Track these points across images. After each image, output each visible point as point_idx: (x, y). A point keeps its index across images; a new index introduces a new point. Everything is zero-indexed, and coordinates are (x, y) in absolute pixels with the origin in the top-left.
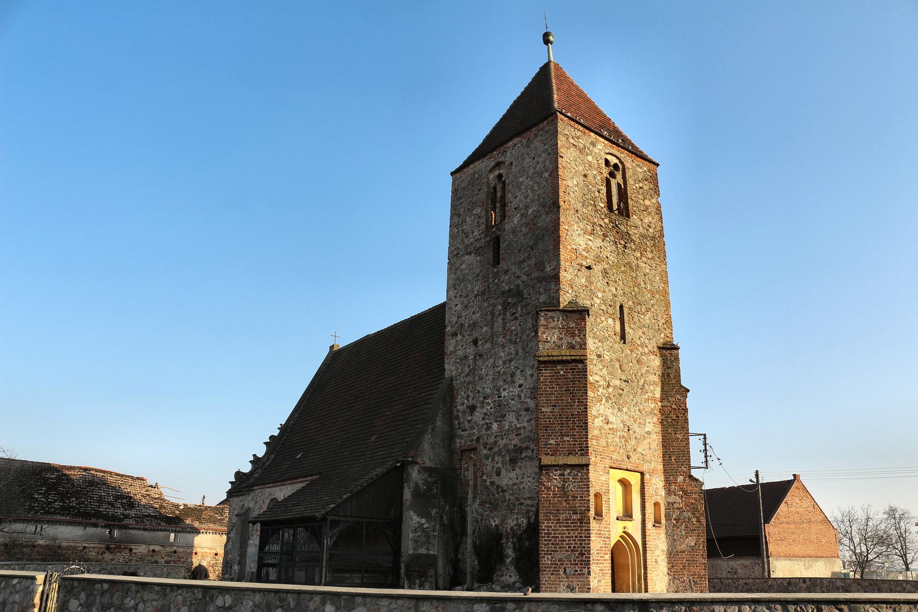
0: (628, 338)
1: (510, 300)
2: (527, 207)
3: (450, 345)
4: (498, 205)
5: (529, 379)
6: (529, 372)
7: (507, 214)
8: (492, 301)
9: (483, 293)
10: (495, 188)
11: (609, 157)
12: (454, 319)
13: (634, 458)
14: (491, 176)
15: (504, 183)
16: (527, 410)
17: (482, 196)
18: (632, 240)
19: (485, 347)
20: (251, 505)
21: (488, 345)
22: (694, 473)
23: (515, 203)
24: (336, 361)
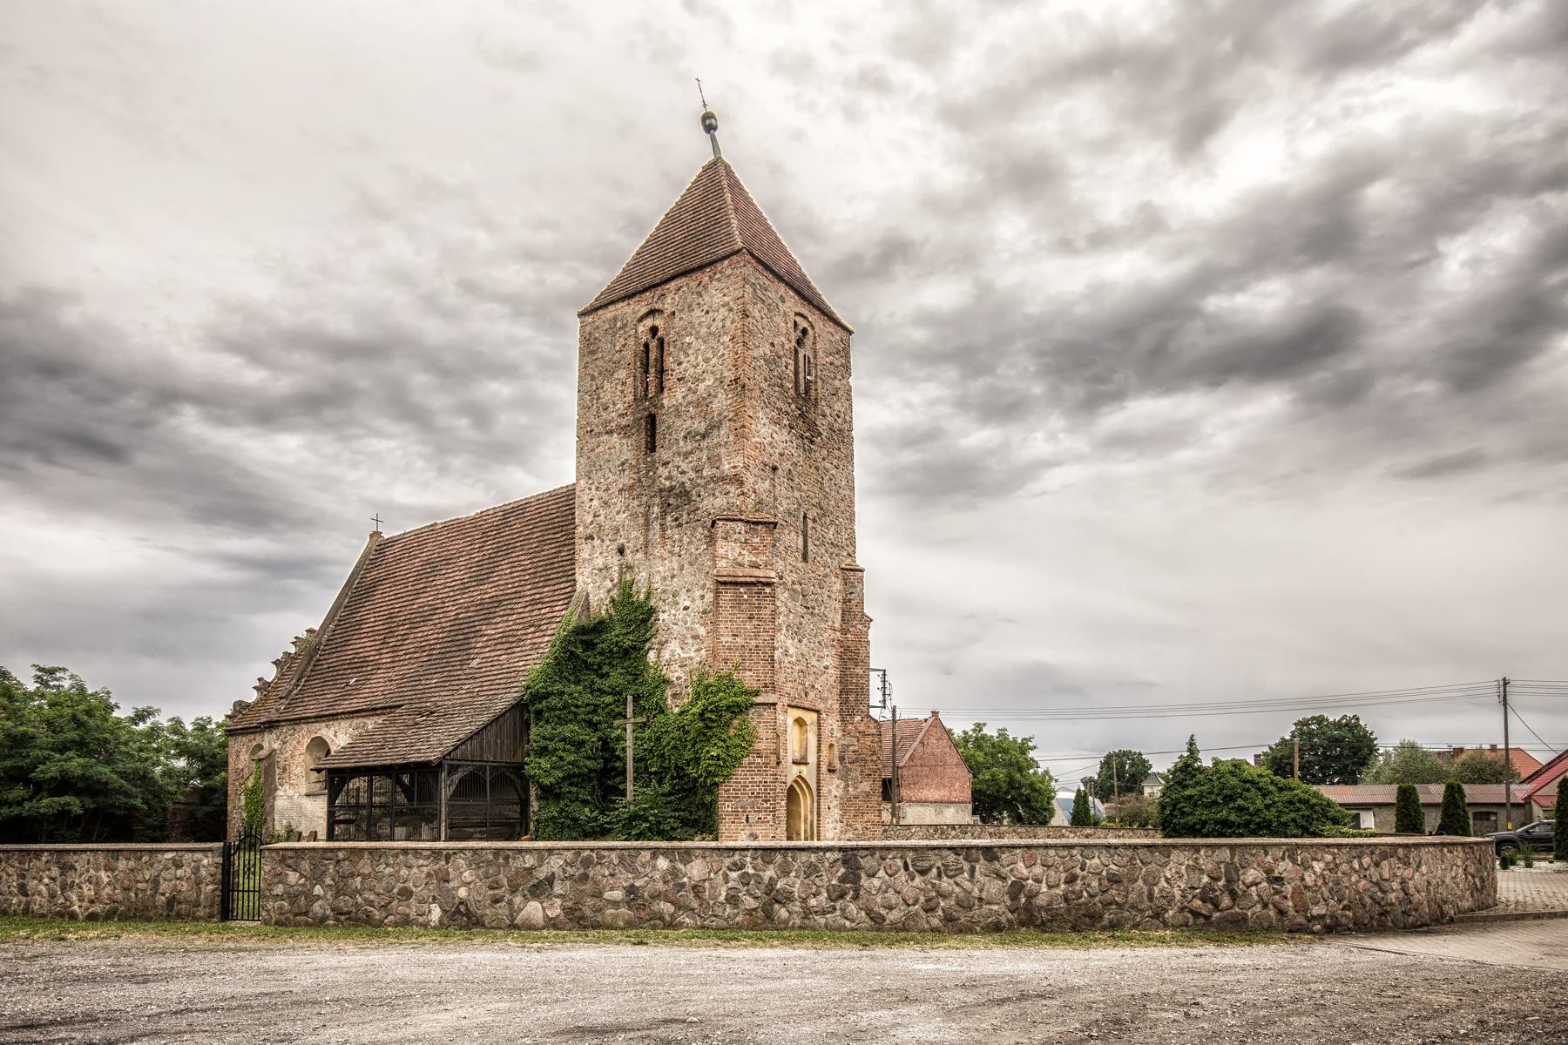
0: (811, 555)
1: (671, 501)
2: (698, 380)
3: (584, 551)
4: (652, 370)
5: (698, 602)
6: (698, 593)
7: (666, 384)
8: (644, 499)
9: (631, 487)
10: (646, 346)
11: (799, 319)
13: (812, 695)
15: (661, 341)
16: (695, 637)
17: (628, 354)
20: (276, 746)
21: (640, 555)
23: (678, 370)
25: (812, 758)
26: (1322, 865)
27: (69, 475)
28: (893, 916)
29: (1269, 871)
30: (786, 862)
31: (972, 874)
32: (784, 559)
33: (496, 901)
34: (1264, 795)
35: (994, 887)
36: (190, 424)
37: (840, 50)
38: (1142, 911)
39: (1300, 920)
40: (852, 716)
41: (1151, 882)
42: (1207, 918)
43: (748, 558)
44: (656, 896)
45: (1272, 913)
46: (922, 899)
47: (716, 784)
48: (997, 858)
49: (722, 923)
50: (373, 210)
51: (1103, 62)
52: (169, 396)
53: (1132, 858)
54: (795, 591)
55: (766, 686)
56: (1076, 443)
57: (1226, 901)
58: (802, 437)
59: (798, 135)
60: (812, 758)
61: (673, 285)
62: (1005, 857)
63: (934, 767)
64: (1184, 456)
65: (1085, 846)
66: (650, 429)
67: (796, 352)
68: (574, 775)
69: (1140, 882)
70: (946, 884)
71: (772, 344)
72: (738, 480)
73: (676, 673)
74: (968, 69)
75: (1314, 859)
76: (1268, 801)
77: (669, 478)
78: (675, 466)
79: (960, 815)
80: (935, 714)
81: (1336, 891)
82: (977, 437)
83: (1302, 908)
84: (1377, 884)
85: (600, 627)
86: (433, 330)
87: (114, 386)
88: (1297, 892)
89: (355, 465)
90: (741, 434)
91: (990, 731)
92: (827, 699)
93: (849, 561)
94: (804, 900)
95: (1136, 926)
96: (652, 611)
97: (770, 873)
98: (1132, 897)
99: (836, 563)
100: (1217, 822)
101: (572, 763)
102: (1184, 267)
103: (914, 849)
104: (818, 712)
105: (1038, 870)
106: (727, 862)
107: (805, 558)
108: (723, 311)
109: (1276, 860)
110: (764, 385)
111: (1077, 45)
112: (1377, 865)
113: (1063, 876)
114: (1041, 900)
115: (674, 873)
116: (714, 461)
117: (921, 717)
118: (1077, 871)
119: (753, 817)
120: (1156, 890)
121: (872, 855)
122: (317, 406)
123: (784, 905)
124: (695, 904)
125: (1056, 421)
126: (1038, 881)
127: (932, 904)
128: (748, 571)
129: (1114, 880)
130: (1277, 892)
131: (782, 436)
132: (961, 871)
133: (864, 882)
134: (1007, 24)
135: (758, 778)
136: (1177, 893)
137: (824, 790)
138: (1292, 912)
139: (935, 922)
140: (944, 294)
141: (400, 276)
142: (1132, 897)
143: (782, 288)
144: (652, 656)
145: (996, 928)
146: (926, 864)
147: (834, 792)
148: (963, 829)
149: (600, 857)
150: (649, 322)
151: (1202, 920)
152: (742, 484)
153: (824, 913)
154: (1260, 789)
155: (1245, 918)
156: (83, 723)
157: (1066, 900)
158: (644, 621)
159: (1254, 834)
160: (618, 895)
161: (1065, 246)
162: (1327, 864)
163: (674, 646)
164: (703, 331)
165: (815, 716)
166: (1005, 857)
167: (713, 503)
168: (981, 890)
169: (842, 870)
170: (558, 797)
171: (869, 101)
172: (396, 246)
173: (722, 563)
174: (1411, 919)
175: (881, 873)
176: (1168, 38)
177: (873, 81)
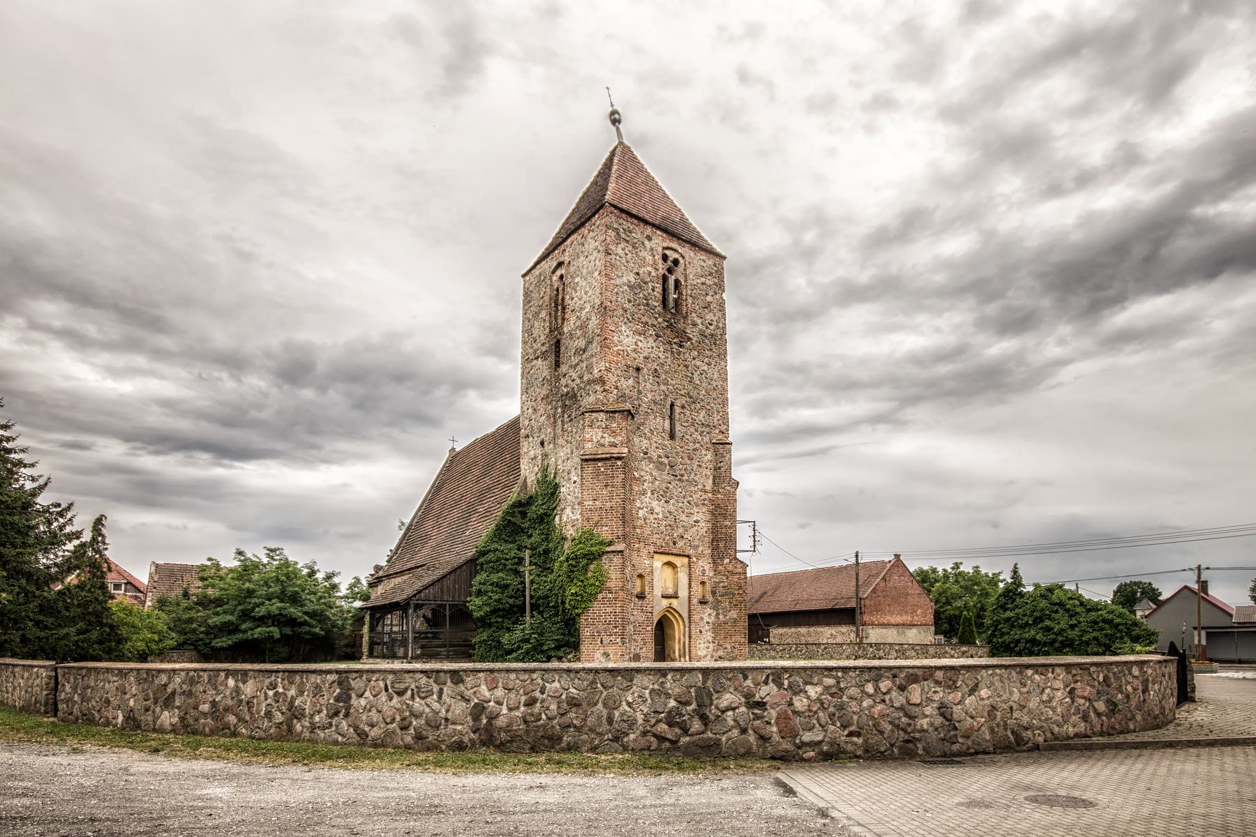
2: (582, 309)
11: (668, 252)
12: (527, 423)
13: (680, 543)
14: (555, 278)
18: (689, 339)
19: (549, 447)
22: (739, 556)
24: (455, 459)
25: (683, 593)
26: (819, 689)
28: (374, 733)
29: (748, 696)
30: (302, 683)
31: (440, 697)
32: (649, 439)
33: (147, 710)
34: (1071, 616)
35: (459, 708)
37: (857, 85)
38: (600, 734)
39: (786, 745)
40: (722, 559)
41: (611, 705)
42: (674, 742)
43: (608, 439)
44: (227, 710)
45: (752, 738)
46: (398, 718)
47: (578, 615)
48: (462, 681)
49: (262, 734)
51: (1072, 46)
53: (593, 682)
54: (661, 463)
55: (618, 537)
56: (1086, 343)
57: (696, 725)
58: (670, 343)
59: (832, 152)
60: (683, 593)
61: (569, 241)
62: (469, 680)
63: (898, 599)
64: (1184, 344)
65: (546, 670)
66: (556, 348)
67: (665, 279)
68: (499, 610)
69: (600, 705)
70: (418, 704)
71: (638, 274)
72: (602, 381)
73: (570, 532)
74: (957, 77)
75: (806, 683)
76: (1074, 622)
77: (566, 386)
78: (571, 377)
79: (927, 636)
80: (897, 556)
81: (840, 716)
82: (999, 348)
83: (789, 732)
84: (901, 708)
85: (531, 500)
88: (783, 718)
90: (605, 344)
91: (967, 568)
92: (697, 547)
93: (720, 437)
94: (312, 716)
95: (594, 749)
96: (557, 486)
97: (292, 692)
98: (591, 721)
99: (707, 439)
100: (1027, 641)
101: (498, 601)
102: (1168, 188)
103: (393, 672)
104: (688, 556)
105: (500, 692)
106: (267, 681)
107: (672, 436)
108: (595, 253)
109: (757, 684)
110: (627, 306)
111: (1045, 39)
113: (523, 699)
114: (501, 722)
115: (237, 690)
116: (589, 368)
117: (887, 560)
118: (537, 694)
119: (606, 640)
120: (617, 713)
121: (361, 677)
123: (299, 720)
124: (248, 718)
125: (1065, 330)
126: (499, 703)
127: (406, 723)
128: (607, 450)
129: (574, 703)
130: (757, 717)
131: (648, 345)
132: (431, 692)
133: (354, 701)
134: (989, 34)
135: (608, 610)
136: (640, 718)
137: (696, 617)
138: (776, 738)
139: (408, 739)
140: (957, 245)
142: (591, 721)
143: (649, 230)
144: (557, 518)
145: (460, 747)
146: (402, 686)
147: (706, 619)
148: (922, 650)
149: (200, 677)
150: (558, 273)
151: (667, 744)
152: (604, 383)
153: (324, 728)
154: (1068, 611)
155: (717, 743)
156: (288, 585)
157: (526, 722)
158: (553, 494)
159: (1059, 651)
160: (205, 707)
161: (1054, 190)
162: (827, 688)
163: (568, 510)
164: (585, 271)
165: (686, 560)
166: (469, 680)
167: (588, 401)
168: (447, 711)
169: (338, 691)
170: (490, 625)
171: (883, 118)
173: (589, 445)
175: (367, 694)
176: (1128, 16)
177: (883, 103)
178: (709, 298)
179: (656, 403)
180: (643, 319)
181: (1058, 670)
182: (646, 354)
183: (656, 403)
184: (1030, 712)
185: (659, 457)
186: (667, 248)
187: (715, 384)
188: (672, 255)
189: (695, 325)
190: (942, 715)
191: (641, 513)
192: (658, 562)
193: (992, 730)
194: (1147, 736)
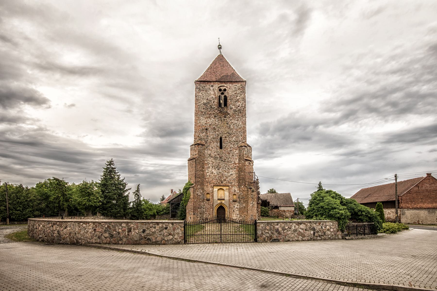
18: (229, 114)
27: (303, 144)
36: (321, 128)
40: (241, 186)
50: (347, 68)
52: (316, 125)
54: (216, 157)
86: (373, 89)
87: (306, 126)
89: (361, 127)
99: (236, 146)
112: (52, 226)
122: (348, 116)
141: (358, 80)
147: (236, 206)
165: (228, 187)
172: (357, 73)
174: (61, 242)
178: (238, 98)
179: (214, 138)
180: (209, 113)
181: (90, 223)
182: (210, 124)
183: (214, 138)
184: (81, 234)
185: (215, 155)
186: (220, 87)
187: (240, 126)
188: (222, 88)
189: (231, 108)
190: (58, 233)
191: (208, 174)
192: (216, 189)
193: (70, 239)
194: (107, 246)
